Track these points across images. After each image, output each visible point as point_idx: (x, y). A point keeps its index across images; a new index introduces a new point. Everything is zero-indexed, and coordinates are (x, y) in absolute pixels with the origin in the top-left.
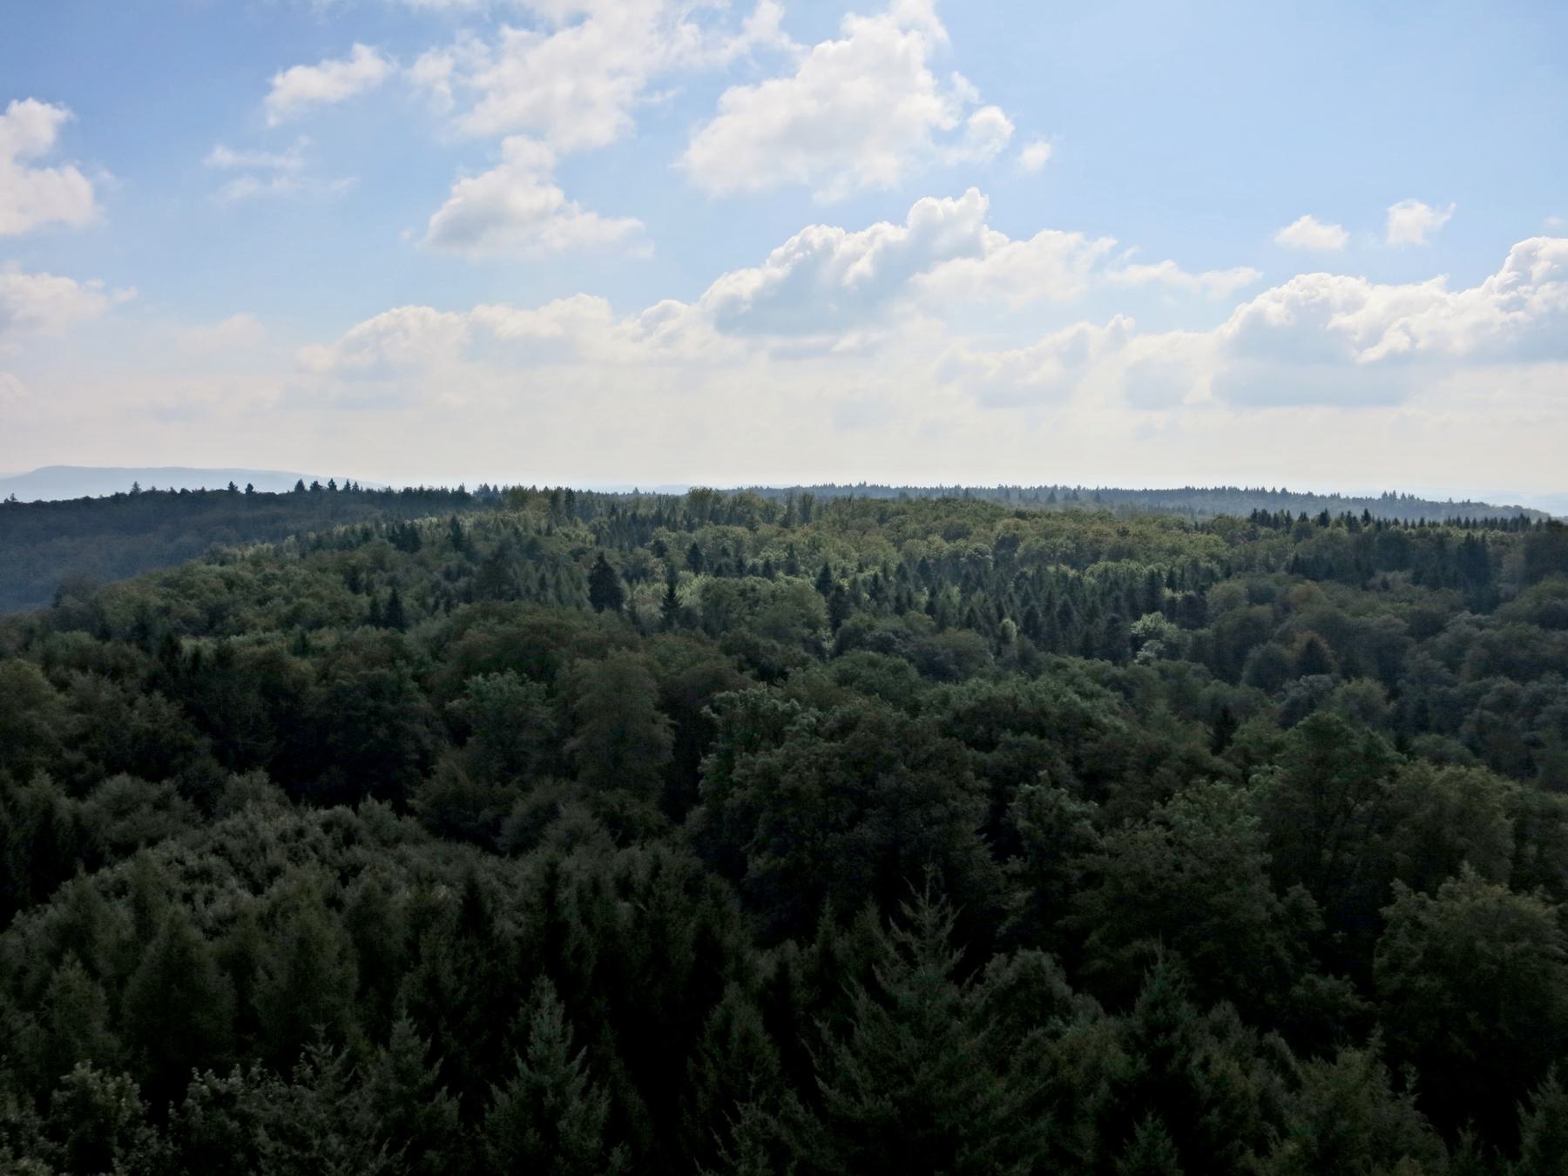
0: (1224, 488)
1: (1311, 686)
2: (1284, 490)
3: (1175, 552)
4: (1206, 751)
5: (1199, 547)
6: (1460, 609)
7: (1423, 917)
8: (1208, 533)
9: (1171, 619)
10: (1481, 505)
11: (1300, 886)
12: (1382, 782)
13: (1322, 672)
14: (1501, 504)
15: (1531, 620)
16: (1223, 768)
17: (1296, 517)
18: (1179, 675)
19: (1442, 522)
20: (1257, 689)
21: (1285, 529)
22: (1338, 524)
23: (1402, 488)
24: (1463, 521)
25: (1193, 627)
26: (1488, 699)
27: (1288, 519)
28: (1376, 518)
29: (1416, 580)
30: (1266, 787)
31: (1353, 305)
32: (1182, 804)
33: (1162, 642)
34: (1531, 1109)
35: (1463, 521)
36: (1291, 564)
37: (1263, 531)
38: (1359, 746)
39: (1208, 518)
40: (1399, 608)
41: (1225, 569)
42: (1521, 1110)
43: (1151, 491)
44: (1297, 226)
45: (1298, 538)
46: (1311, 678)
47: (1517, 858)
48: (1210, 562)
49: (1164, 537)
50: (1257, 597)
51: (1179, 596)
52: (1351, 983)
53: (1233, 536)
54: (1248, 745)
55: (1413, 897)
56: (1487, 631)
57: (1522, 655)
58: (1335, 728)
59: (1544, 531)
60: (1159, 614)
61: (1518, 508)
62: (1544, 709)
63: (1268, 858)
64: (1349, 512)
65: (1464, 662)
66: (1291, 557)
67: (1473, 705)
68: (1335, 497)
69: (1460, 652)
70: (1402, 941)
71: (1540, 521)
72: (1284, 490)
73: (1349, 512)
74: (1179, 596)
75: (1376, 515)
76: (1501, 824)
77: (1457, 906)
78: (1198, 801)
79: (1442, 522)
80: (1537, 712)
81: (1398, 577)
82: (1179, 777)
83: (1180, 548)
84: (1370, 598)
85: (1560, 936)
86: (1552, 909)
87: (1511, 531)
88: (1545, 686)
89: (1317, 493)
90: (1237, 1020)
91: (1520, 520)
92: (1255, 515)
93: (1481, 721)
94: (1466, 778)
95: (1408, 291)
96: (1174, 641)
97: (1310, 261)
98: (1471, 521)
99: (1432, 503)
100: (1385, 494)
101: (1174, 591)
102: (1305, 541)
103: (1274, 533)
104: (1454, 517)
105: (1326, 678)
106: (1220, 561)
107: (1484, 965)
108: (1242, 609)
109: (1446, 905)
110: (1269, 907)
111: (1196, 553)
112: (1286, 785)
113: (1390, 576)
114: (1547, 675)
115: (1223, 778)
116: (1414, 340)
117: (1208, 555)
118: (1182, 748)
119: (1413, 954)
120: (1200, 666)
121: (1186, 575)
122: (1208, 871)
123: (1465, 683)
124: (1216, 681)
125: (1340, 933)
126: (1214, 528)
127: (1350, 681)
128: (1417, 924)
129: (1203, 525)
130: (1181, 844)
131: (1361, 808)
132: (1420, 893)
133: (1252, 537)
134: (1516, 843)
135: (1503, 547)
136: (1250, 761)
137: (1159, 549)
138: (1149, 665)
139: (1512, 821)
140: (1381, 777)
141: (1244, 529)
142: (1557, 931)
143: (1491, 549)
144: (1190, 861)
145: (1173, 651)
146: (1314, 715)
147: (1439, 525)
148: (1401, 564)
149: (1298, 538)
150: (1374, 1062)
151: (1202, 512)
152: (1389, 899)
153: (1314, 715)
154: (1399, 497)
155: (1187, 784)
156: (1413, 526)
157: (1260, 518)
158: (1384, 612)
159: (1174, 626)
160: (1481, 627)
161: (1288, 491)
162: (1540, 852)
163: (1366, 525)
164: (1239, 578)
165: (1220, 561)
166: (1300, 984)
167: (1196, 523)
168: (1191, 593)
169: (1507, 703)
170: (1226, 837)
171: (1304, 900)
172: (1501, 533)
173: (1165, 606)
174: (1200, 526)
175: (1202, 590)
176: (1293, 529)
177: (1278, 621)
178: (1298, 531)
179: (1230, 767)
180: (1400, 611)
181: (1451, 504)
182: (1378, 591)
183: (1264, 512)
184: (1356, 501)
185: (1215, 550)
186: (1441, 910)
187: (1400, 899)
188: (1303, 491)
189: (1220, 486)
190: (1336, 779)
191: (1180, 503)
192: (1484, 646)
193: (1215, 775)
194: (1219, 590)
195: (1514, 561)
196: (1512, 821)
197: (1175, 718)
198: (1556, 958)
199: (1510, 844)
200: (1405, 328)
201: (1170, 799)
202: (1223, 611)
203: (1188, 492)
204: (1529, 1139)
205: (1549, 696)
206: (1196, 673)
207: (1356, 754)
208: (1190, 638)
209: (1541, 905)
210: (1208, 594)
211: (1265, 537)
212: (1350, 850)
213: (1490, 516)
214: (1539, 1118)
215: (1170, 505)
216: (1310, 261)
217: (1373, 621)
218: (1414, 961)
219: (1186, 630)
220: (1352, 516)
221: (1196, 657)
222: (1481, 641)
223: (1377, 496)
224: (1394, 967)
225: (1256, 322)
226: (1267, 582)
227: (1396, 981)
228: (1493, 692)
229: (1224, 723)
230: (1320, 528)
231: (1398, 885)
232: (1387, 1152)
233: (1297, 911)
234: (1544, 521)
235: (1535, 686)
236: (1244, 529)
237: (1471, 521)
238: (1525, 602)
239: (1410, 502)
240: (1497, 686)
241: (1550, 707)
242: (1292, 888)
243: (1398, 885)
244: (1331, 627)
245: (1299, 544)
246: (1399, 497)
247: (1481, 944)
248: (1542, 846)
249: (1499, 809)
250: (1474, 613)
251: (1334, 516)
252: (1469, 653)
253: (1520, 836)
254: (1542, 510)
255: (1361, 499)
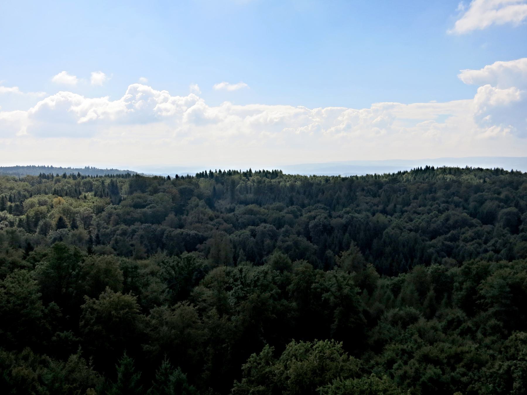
0: (30, 166)
1: (61, 233)
2: (52, 166)
3: (11, 189)
4: (20, 260)
5: (20, 187)
6: (109, 204)
7: (95, 307)
8: (24, 182)
9: (10, 213)
10: (117, 170)
11: (53, 303)
12: (80, 263)
13: (65, 228)
14: (122, 170)
15: (131, 206)
16: (25, 265)
17: (55, 175)
18: (13, 232)
19: (103, 176)
20: (42, 235)
21: (51, 179)
22: (70, 177)
23: (91, 165)
24: (110, 175)
25: (18, 215)
26: (118, 232)
27: (53, 176)
28: (82, 175)
29: (95, 196)
30: (41, 269)
31: (78, 104)
32: (10, 279)
33: (7, 221)
34: (120, 366)
35: (110, 175)
36: (53, 191)
37: (44, 180)
38: (72, 252)
39: (24, 176)
40: (89, 204)
41: (30, 194)
42: (117, 366)
43: (4, 167)
44: (60, 75)
45: (56, 183)
46: (60, 230)
47: (125, 283)
48: (24, 192)
49: (8, 184)
50: (41, 204)
51: (13, 204)
52: (72, 332)
53: (33, 182)
54: (35, 256)
55: (91, 300)
56: (117, 210)
57: (129, 217)
58: (63, 247)
59: (135, 178)
60: (6, 211)
61: (128, 171)
62: (136, 234)
63: (40, 294)
64: (73, 173)
65: (111, 221)
66: (53, 189)
67: (114, 235)
68: (69, 168)
69: (109, 218)
70: (88, 315)
71: (133, 175)
72: (52, 166)
73: (73, 173)
74: (13, 204)
75: (82, 174)
76: (119, 273)
77: (105, 301)
78: (15, 278)
79: (103, 176)
80: (134, 235)
81: (90, 195)
82: (9, 270)
83: (14, 187)
84: (81, 202)
85: (138, 306)
86: (135, 298)
87: (125, 178)
88: (135, 226)
89: (63, 167)
90: (32, 353)
91: (128, 175)
92: (40, 175)
93: (116, 239)
94: (107, 259)
95: (96, 100)
96: (12, 220)
97: (65, 87)
98: (113, 175)
99: (101, 170)
100: (86, 167)
101: (11, 203)
102: (58, 183)
103: (48, 181)
104: (107, 174)
105: (66, 229)
106: (28, 192)
107: (114, 319)
108: (37, 207)
109: (102, 301)
110: (42, 311)
111: (20, 189)
112: (48, 268)
113: (86, 194)
114: (136, 223)
115: (26, 268)
116: (98, 116)
117: (24, 189)
118: (10, 259)
119: (92, 319)
120: (21, 229)
121: (16, 197)
122: (19, 302)
123: (111, 228)
124: (27, 233)
125: (68, 316)
126: (26, 180)
127: (74, 230)
128: (93, 309)
129: (22, 179)
130: (10, 293)
131: (74, 273)
132: (93, 299)
133: (40, 182)
134: (124, 278)
135: (122, 183)
136: (36, 261)
137: (6, 188)
138: (2, 230)
139: (122, 271)
140: (79, 262)
141: (37, 180)
142: (137, 304)
143: (119, 184)
144: (12, 299)
145: (12, 224)
146: (56, 243)
147: (102, 177)
148: (90, 190)
149: (56, 183)
150: (80, 357)
151: (22, 174)
152: (84, 302)
153: (56, 243)
154: (90, 168)
155: (12, 272)
156: (94, 177)
157: (42, 176)
158: (85, 206)
159: (12, 215)
160: (115, 209)
161: (53, 166)
162: (132, 280)
163: (79, 177)
164: (35, 197)
165: (28, 192)
166: (55, 336)
167: (20, 179)
168: (18, 203)
169: (124, 233)
170: (25, 289)
171: (55, 307)
172: (122, 179)
173: (8, 209)
174: (21, 179)
175: (21, 202)
176: (54, 179)
177: (48, 211)
178: (56, 180)
179: (28, 264)
180: (90, 206)
181: (107, 170)
182: (83, 199)
183: (44, 174)
184: (76, 169)
185: (26, 188)
186: (100, 303)
187: (87, 302)
188: (58, 166)
189: (29, 165)
190: (65, 264)
191: (15, 171)
192: (117, 215)
193: (23, 267)
194: (28, 201)
195: (126, 187)
196: (122, 271)
197: (11, 248)
198: (137, 313)
199: (122, 279)
200: (95, 112)
201: (5, 278)
202: (29, 209)
203: (17, 168)
204: (120, 375)
205: (137, 230)
206: (20, 231)
207: (71, 255)
208: (17, 219)
209: (131, 297)
210: (24, 203)
211: (44, 182)
212: (71, 287)
213: (118, 173)
214: (122, 368)
215: (11, 172)
216: (65, 87)
217: (82, 210)
218: (92, 321)
219: (16, 216)
220: (74, 174)
221: (19, 226)
222: (116, 214)
223: (83, 168)
224: (85, 325)
225: (45, 107)
226: (45, 198)
227: (87, 330)
228: (120, 230)
229: (29, 248)
230: (63, 179)
231: (86, 297)
232: (84, 386)
233: (52, 310)
234: (135, 174)
235: (133, 227)
236: (37, 180)
237: (113, 175)
238: (129, 201)
239: (94, 169)
240: (121, 228)
241: (137, 233)
242: (50, 303)
243: (86, 297)
244: (66, 211)
245: (56, 185)
246: (90, 168)
247: (113, 312)
248: (133, 278)
249: (118, 268)
250: (113, 205)
251: (68, 175)
252: (112, 218)
253: (125, 275)
254: (135, 171)
255: (78, 169)
